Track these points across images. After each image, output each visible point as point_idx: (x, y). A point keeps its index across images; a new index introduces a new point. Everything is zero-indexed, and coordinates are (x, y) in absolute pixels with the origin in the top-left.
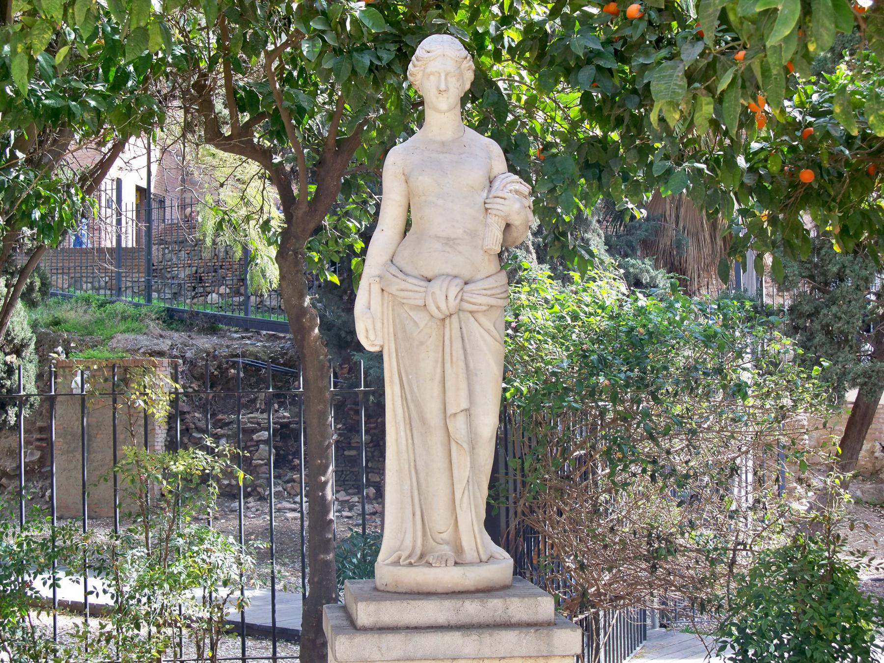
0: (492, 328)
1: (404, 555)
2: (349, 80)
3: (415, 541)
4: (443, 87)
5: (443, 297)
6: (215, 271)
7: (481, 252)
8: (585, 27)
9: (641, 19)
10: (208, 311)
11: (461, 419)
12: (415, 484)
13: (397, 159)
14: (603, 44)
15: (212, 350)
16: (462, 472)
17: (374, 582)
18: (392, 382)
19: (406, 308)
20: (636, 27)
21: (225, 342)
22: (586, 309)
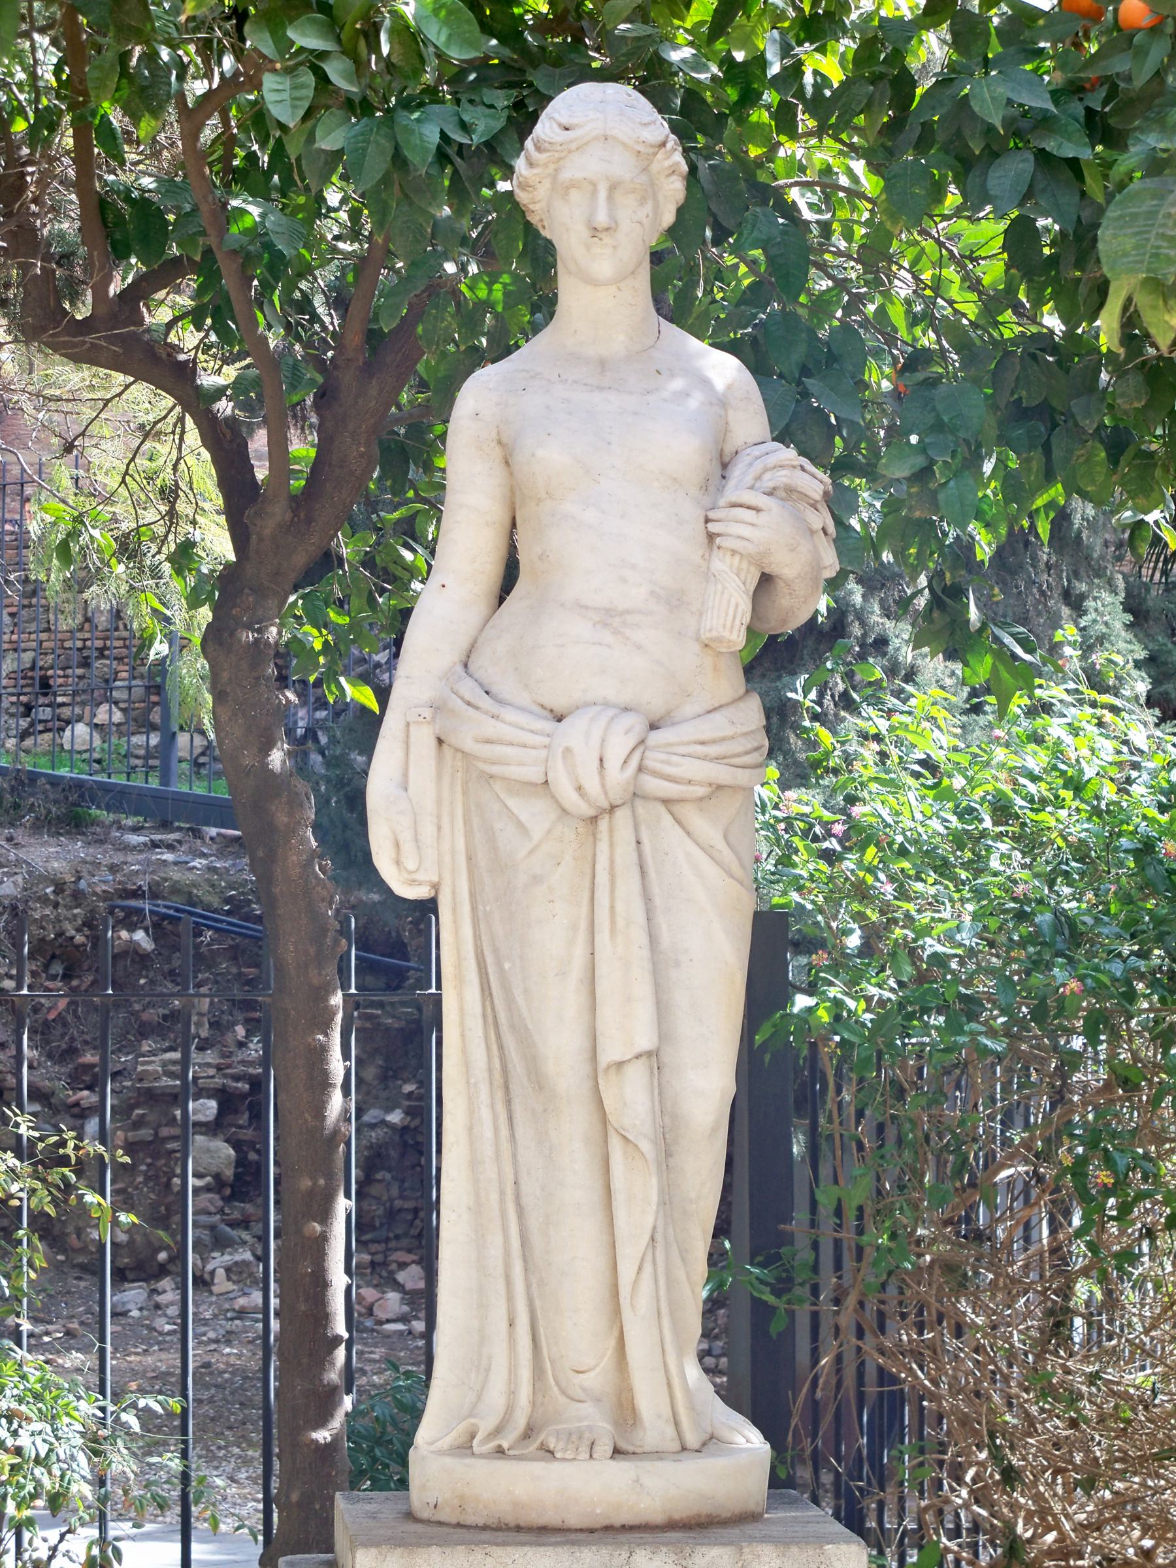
0: (721, 845)
1: (485, 1426)
2: (386, 180)
3: (512, 1393)
4: (602, 218)
5: (593, 755)
6: (86, 663)
7: (696, 647)
8: (1012, 50)
9: (1154, 30)
10: (64, 772)
11: (636, 1080)
12: (515, 1243)
13: (480, 397)
14: (1056, 95)
15: (70, 878)
16: (637, 1218)
17: (408, 1498)
18: (460, 979)
19: (498, 786)
20: (1141, 53)
21: (105, 856)
22: (1032, 788)
